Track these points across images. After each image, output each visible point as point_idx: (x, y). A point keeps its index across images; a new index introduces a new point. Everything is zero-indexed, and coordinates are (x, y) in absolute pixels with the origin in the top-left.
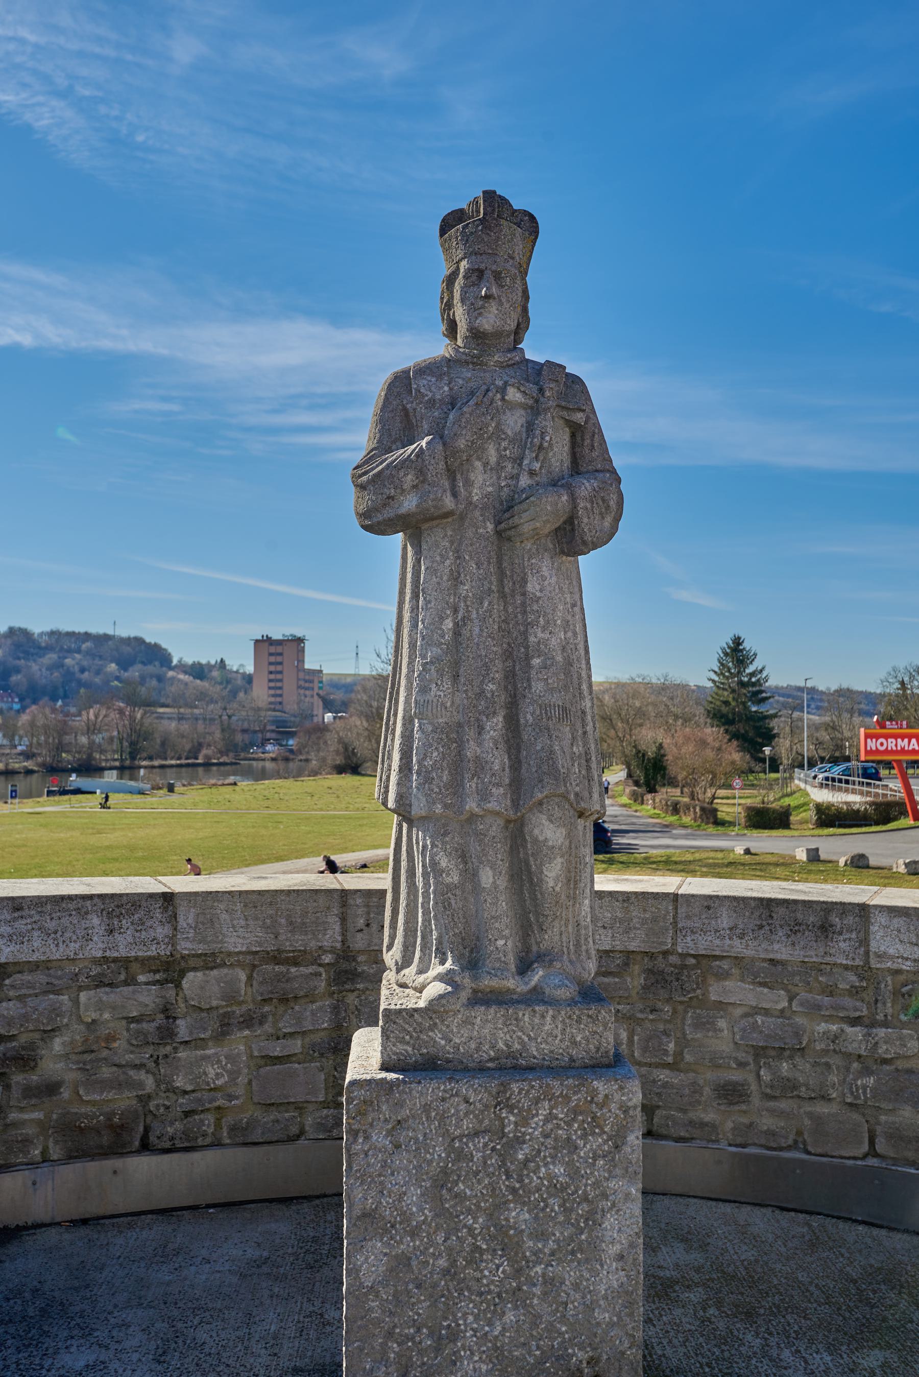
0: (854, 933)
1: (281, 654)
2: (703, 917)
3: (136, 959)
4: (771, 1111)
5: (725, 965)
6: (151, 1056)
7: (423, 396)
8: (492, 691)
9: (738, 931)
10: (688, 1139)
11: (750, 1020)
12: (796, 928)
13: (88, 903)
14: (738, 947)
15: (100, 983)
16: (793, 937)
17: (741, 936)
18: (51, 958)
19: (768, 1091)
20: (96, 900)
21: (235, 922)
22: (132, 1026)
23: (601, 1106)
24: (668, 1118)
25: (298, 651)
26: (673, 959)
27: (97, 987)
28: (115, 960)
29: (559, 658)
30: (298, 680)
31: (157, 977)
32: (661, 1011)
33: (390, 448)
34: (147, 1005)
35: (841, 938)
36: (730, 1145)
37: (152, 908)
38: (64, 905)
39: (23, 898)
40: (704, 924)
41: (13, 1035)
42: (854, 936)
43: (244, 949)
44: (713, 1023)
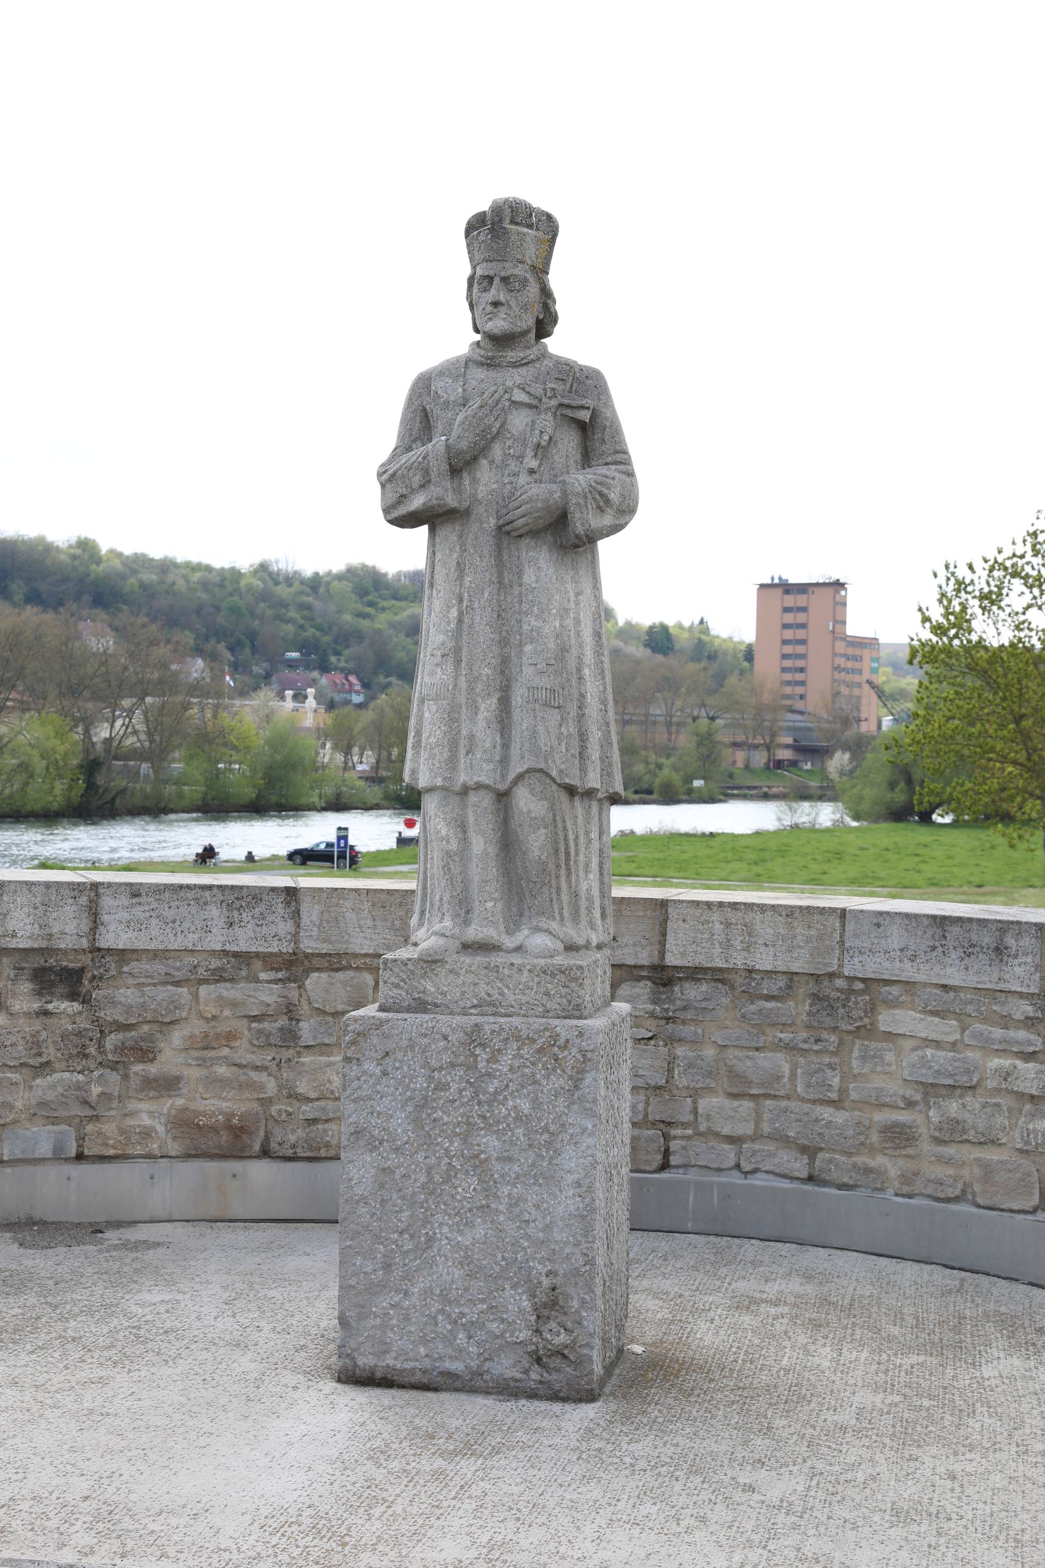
0: (1030, 956)
1: (804, 609)
2: (872, 935)
3: (257, 955)
4: (940, 1159)
5: (895, 990)
6: (274, 1059)
7: (439, 397)
8: (487, 675)
9: (910, 953)
10: (852, 1186)
11: (919, 1053)
12: (970, 950)
13: (207, 893)
14: (908, 971)
15: (219, 977)
16: (967, 960)
17: (913, 959)
18: (169, 948)
19: (937, 1134)
20: (215, 891)
21: (362, 922)
22: (254, 1025)
23: (564, 1048)
24: (830, 1161)
25: (836, 603)
26: (840, 983)
27: (217, 981)
28: (236, 955)
29: (552, 645)
30: (835, 655)
31: (280, 975)
32: (827, 1041)
33: (410, 447)
34: (268, 1005)
35: (1016, 962)
36: (897, 1195)
37: (274, 902)
38: (182, 894)
39: (141, 884)
40: (873, 944)
41: (133, 1025)
42: (1029, 959)
43: (371, 952)
44: (882, 1058)
